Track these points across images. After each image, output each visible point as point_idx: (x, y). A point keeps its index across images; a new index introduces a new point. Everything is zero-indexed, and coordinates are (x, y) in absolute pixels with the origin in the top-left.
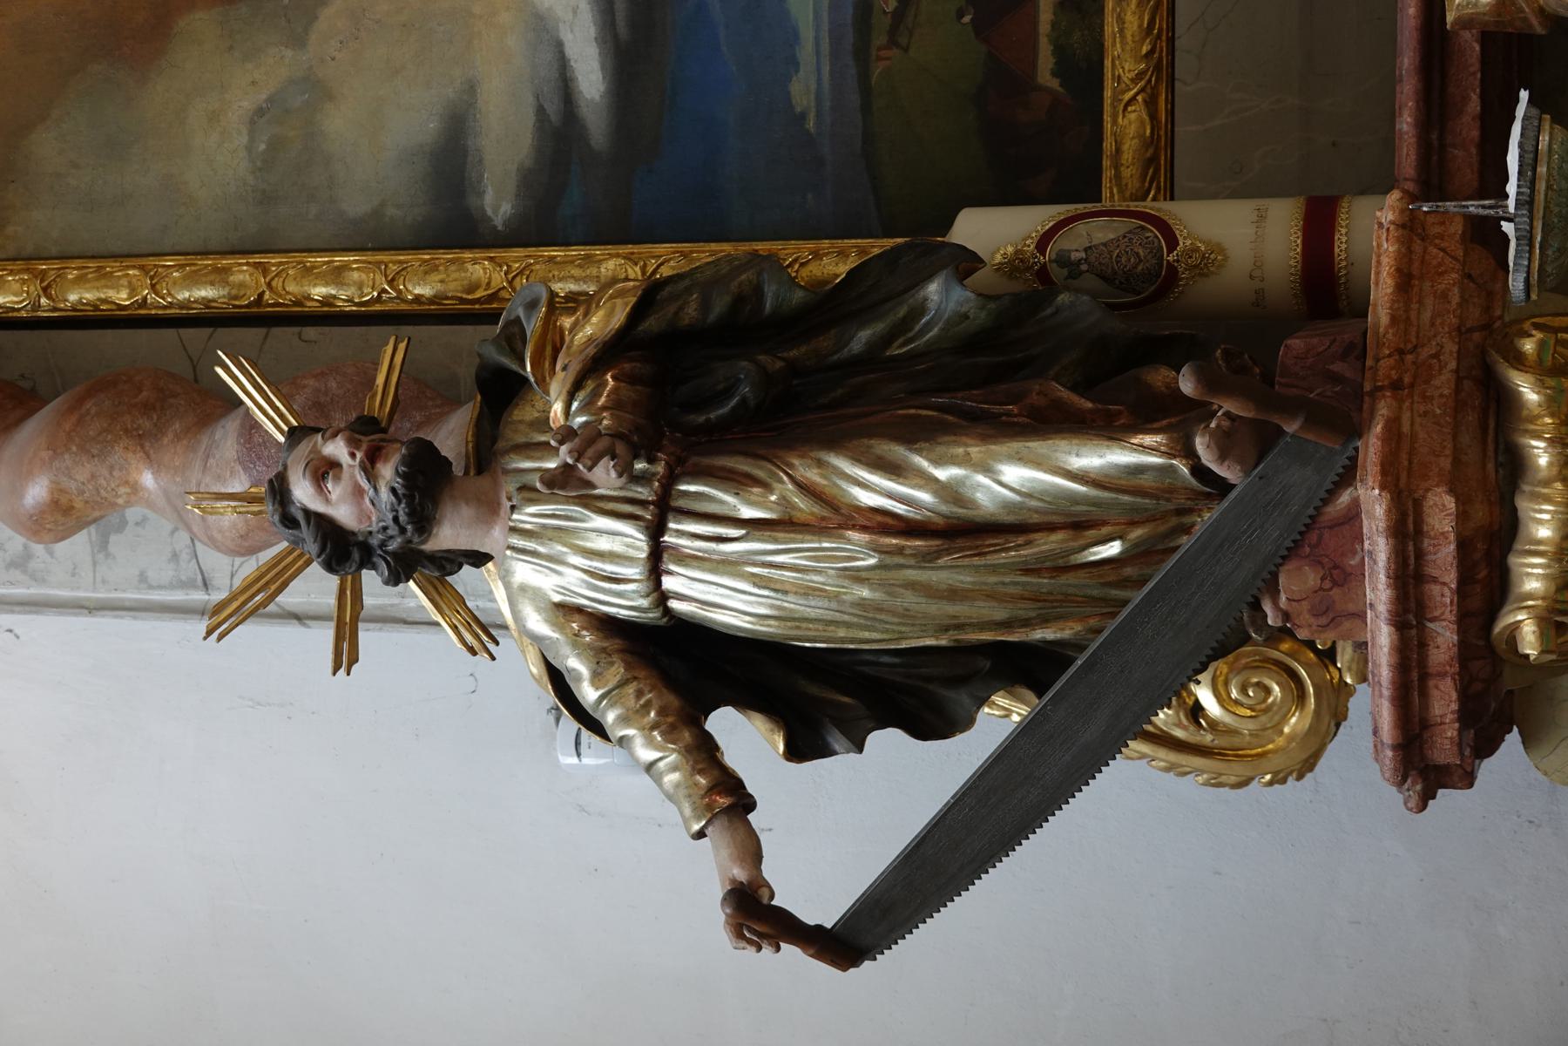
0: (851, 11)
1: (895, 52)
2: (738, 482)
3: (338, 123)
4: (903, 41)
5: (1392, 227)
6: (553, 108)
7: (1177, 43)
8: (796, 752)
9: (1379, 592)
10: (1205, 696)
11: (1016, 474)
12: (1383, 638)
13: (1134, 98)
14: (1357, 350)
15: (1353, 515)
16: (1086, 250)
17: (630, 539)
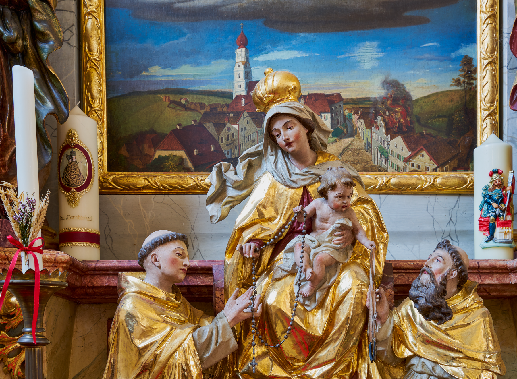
0: (181, 87)
1: (167, 103)
4: (171, 105)
5: (55, 256)
7: (167, 195)
13: (149, 182)
16: (76, 161)
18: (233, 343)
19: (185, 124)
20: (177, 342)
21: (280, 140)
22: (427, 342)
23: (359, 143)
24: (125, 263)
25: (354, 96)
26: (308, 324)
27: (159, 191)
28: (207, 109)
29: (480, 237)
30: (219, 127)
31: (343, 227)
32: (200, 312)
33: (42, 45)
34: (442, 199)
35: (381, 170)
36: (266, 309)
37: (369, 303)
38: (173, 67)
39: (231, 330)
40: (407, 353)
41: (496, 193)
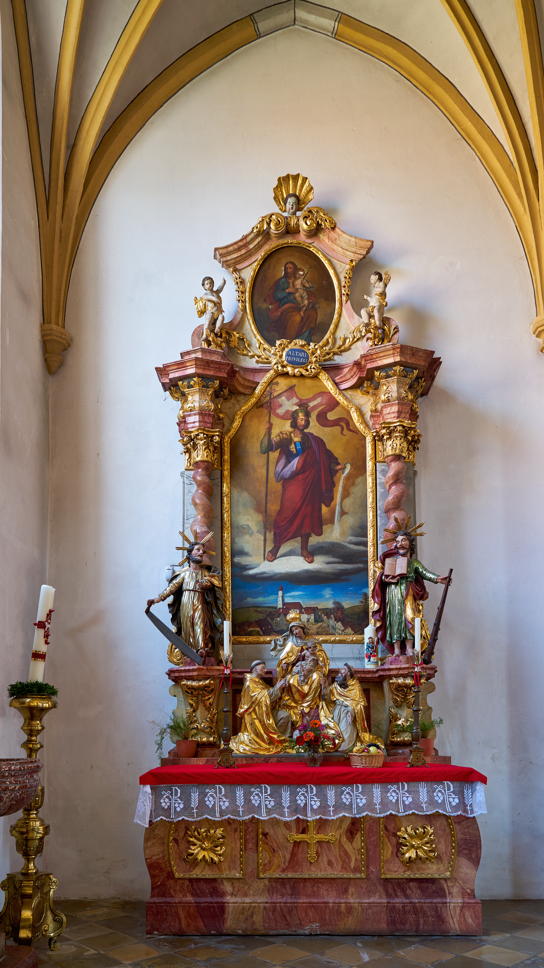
2: (198, 600)
3: (247, 537)
6: (248, 567)
8: (169, 605)
9: (187, 668)
10: (177, 650)
11: (199, 630)
12: (183, 669)
14: (212, 665)
15: (195, 665)
17: (191, 587)
18: (280, 694)
19: (260, 618)
20: (263, 694)
21: (294, 632)
22: (340, 695)
23: (325, 625)
24: (245, 670)
25: (322, 608)
26: (303, 689)
27: (250, 643)
28: (268, 613)
29: (366, 660)
30: (272, 619)
31: (313, 659)
32: (268, 686)
33: (218, 601)
34: (356, 645)
35: (333, 634)
36: (290, 685)
37: (322, 683)
38: (256, 598)
39: (147, 870)
40: (335, 699)
41: (371, 645)
